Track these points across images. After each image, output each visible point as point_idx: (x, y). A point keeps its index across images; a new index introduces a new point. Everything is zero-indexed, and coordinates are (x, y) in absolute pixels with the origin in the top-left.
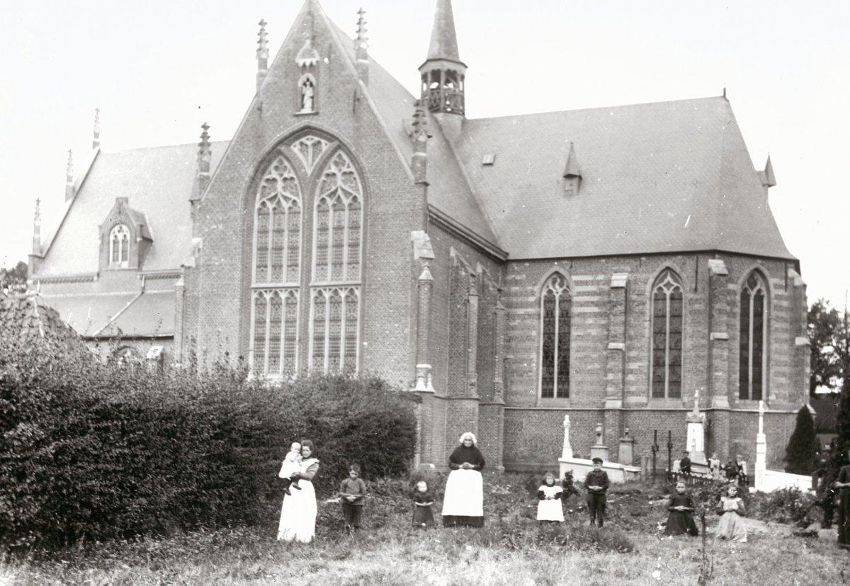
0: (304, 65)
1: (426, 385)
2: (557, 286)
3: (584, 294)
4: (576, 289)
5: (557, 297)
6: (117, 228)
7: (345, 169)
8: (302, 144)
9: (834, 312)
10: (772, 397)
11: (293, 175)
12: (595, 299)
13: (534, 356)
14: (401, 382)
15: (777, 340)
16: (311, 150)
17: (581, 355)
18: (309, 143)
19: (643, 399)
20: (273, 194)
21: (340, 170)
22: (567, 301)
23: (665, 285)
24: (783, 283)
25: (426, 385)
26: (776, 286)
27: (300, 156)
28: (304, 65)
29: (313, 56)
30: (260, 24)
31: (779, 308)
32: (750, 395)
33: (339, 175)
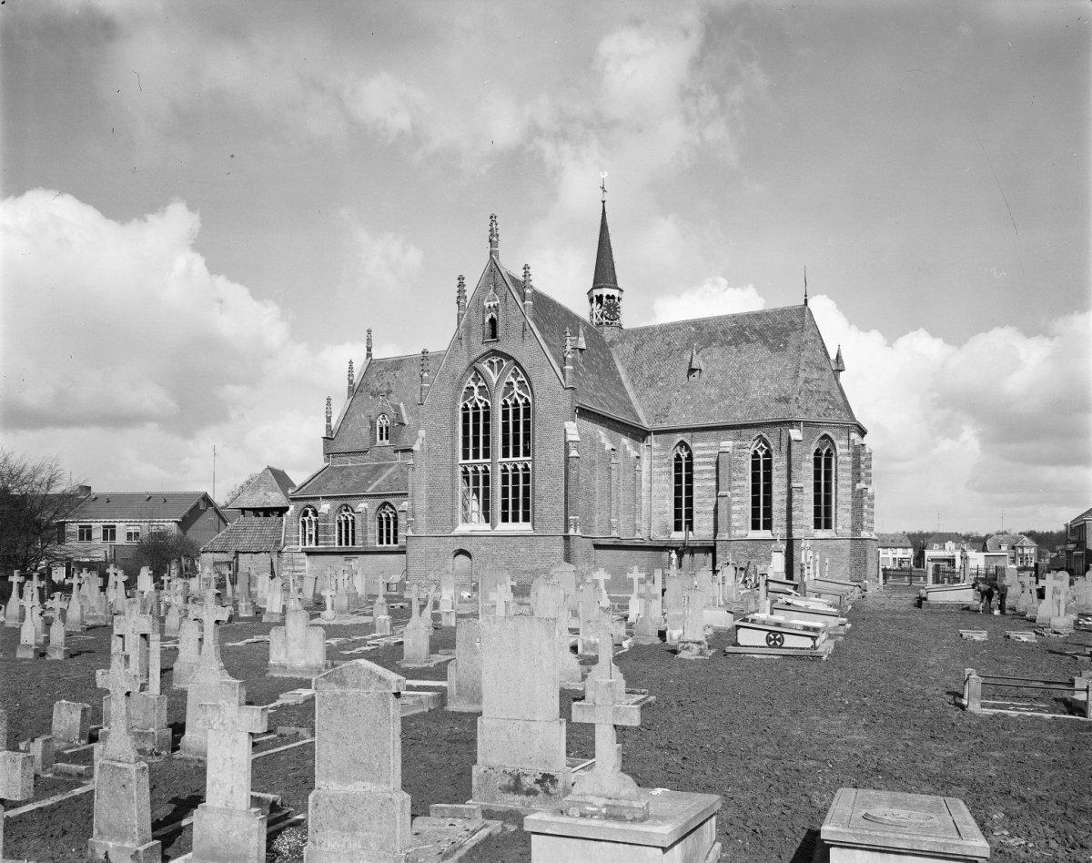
0: (490, 307)
1: (575, 531)
2: (683, 451)
3: (702, 456)
4: (696, 453)
5: (683, 458)
6: (381, 416)
7: (519, 379)
8: (490, 361)
9: (666, 218)
10: (840, 528)
11: (484, 384)
12: (707, 460)
13: (667, 502)
14: (368, 693)
15: (843, 486)
16: (496, 365)
17: (701, 500)
18: (494, 361)
19: (743, 532)
20: (471, 398)
21: (476, 384)
22: (690, 457)
25: (575, 531)
28: (490, 307)
29: (495, 300)
30: (459, 279)
31: (845, 463)
32: (871, 510)
33: (476, 388)
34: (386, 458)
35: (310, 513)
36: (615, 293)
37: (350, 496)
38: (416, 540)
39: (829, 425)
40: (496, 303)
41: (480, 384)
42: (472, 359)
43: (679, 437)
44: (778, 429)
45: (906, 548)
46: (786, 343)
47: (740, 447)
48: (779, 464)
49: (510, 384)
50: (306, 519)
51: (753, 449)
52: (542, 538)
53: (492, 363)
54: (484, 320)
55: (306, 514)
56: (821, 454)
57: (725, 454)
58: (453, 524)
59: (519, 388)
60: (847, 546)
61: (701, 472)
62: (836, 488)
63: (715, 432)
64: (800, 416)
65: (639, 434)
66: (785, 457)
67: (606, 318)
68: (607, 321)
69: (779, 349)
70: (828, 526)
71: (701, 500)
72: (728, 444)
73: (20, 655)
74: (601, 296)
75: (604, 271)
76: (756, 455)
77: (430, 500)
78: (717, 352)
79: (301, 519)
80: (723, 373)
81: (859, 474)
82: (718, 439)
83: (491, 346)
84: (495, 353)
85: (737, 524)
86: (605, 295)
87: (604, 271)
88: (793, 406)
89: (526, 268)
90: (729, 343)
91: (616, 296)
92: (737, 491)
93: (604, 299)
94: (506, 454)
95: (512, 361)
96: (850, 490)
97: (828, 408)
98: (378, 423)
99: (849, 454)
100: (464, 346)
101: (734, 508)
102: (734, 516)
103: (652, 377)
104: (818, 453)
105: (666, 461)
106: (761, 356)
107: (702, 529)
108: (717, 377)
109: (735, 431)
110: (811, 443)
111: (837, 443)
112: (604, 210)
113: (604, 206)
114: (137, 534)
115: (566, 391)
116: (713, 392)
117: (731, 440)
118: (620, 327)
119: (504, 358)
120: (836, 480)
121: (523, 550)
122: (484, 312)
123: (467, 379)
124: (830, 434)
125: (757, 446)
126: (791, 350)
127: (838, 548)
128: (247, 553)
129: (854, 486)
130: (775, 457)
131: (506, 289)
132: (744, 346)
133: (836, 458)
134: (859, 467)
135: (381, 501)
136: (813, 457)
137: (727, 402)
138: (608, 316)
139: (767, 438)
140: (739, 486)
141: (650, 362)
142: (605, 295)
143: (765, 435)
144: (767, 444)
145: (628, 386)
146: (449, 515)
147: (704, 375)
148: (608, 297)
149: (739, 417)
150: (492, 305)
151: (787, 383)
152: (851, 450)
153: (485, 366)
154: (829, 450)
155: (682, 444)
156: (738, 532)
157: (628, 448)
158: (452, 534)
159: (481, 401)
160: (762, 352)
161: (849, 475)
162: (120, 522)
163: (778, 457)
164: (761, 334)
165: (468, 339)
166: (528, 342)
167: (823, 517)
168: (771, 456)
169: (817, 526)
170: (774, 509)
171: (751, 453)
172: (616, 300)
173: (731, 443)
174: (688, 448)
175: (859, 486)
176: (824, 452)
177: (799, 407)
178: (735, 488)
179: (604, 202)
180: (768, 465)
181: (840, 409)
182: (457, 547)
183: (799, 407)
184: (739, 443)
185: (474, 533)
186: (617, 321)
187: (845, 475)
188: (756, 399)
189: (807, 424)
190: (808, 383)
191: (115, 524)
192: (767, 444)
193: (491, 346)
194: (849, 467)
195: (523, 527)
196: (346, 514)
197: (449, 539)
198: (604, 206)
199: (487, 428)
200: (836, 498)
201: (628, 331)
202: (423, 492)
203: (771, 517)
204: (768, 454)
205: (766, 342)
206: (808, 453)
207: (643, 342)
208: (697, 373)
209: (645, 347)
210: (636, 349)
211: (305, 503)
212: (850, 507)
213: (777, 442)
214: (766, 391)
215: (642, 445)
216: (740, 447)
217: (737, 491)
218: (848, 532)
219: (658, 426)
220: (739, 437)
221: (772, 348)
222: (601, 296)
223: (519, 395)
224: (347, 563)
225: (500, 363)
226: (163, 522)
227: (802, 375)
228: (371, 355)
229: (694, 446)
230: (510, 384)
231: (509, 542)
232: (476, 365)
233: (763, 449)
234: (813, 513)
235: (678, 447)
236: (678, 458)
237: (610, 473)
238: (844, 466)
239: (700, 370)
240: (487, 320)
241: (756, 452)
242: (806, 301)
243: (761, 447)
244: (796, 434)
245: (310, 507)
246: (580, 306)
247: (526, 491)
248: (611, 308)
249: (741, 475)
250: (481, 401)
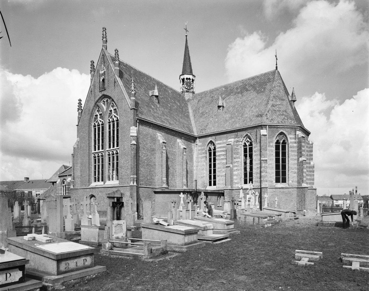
0: (102, 74)
1: (133, 183)
3: (220, 147)
4: (217, 146)
5: (212, 149)
10: (290, 182)
12: (222, 149)
15: (292, 159)
16: (106, 103)
17: (219, 170)
18: (105, 100)
20: (97, 120)
22: (215, 149)
23: (246, 142)
24: (294, 137)
25: (133, 183)
26: (290, 138)
27: (103, 105)
32: (313, 174)
36: (191, 77)
38: (75, 191)
39: (284, 127)
42: (96, 101)
43: (210, 139)
44: (255, 130)
45: (361, 200)
46: (264, 89)
47: (237, 141)
48: (256, 148)
49: (111, 111)
50: (64, 185)
51: (243, 142)
52: (122, 188)
54: (100, 80)
56: (280, 143)
57: (229, 145)
58: (89, 182)
59: (115, 113)
60: (295, 192)
61: (219, 156)
62: (288, 161)
63: (225, 135)
64: (268, 122)
65: (190, 139)
66: (259, 144)
67: (186, 89)
68: (187, 90)
70: (284, 181)
71: (219, 170)
72: (231, 140)
74: (184, 78)
75: (187, 67)
77: (81, 171)
78: (232, 97)
79: (62, 185)
80: (234, 106)
81: (301, 153)
82: (227, 138)
84: (105, 96)
85: (236, 181)
86: (185, 78)
87: (187, 67)
88: (264, 118)
89: (117, 51)
90: (239, 93)
91: (191, 78)
92: (236, 164)
93: (185, 80)
96: (296, 162)
97: (284, 119)
99: (295, 142)
100: (93, 95)
101: (235, 173)
102: (235, 177)
103: (202, 113)
104: (278, 142)
105: (204, 151)
106: (252, 96)
107: (220, 185)
108: (231, 109)
109: (233, 134)
110: (273, 137)
111: (288, 137)
112: (187, 48)
113: (186, 38)
114: (39, 194)
115: (132, 110)
116: (228, 116)
117: (233, 138)
118: (193, 92)
119: (109, 98)
120: (288, 156)
123: (95, 111)
124: (283, 131)
125: (246, 140)
126: (267, 92)
127: (290, 193)
129: (298, 159)
130: (254, 145)
132: (245, 93)
133: (288, 144)
134: (301, 149)
136: (275, 144)
137: (233, 120)
138: (187, 87)
140: (237, 161)
141: (203, 106)
142: (185, 78)
143: (249, 134)
144: (250, 139)
145: (192, 118)
146: (87, 178)
147: (225, 109)
148: (187, 79)
151: (262, 108)
152: (297, 140)
153: (102, 104)
154: (284, 141)
155: (211, 142)
156: (237, 185)
157: (180, 144)
159: (100, 121)
161: (296, 154)
162: (34, 190)
163: (255, 145)
164: (254, 87)
167: (281, 175)
168: (252, 145)
169: (277, 181)
170: (253, 172)
171: (243, 144)
172: (191, 80)
173: (233, 140)
174: (214, 145)
175: (301, 159)
176: (281, 142)
177: (267, 118)
178: (235, 163)
179: (186, 36)
180: (251, 150)
181: (291, 119)
183: (267, 118)
184: (237, 139)
186: (192, 90)
187: (293, 153)
188: (246, 117)
189: (270, 127)
190: (274, 106)
191: (24, 191)
192: (250, 139)
194: (296, 149)
197: (88, 190)
198: (186, 38)
200: (288, 166)
201: (199, 94)
202: (78, 168)
203: (252, 177)
204: (251, 144)
206: (272, 142)
207: (202, 98)
208: (221, 108)
209: (203, 100)
210: (199, 102)
212: (296, 171)
213: (255, 137)
214: (252, 112)
215: (193, 144)
216: (237, 141)
217: (236, 164)
218: (295, 184)
219: (202, 134)
220: (237, 136)
221: (258, 92)
222: (184, 78)
225: (107, 101)
226: (40, 190)
227: (271, 103)
229: (216, 143)
230: (111, 111)
231: (110, 190)
233: (249, 141)
234: (275, 174)
235: (210, 144)
236: (210, 150)
237: (162, 154)
238: (293, 149)
239: (223, 107)
240: (101, 80)
241: (245, 143)
242: (277, 67)
243: (248, 140)
244: (264, 132)
246: (178, 87)
247: (117, 163)
248: (188, 84)
249: (238, 156)
250: (100, 121)
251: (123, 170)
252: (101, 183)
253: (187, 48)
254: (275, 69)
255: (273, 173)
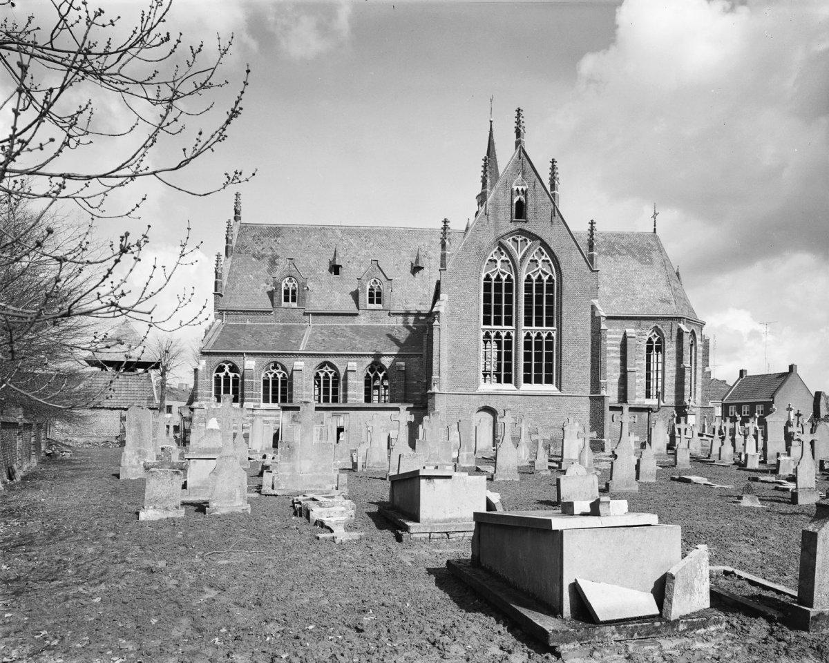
0: (517, 190)
6: (287, 279)
7: (543, 258)
8: (514, 239)
18: (519, 239)
28: (517, 190)
29: (525, 185)
34: (293, 319)
35: (227, 369)
37: (283, 354)
40: (524, 189)
41: (503, 258)
44: (669, 322)
47: (640, 334)
50: (222, 375)
52: (569, 398)
53: (517, 241)
55: (221, 369)
57: (632, 339)
69: (646, 263)
73: (147, 515)
76: (650, 341)
77: (453, 360)
83: (519, 225)
94: (528, 322)
95: (539, 242)
98: (283, 285)
100: (492, 222)
112: (491, 129)
121: (550, 408)
122: (512, 194)
125: (651, 334)
128: (114, 409)
131: (535, 177)
135: (320, 360)
139: (661, 329)
143: (659, 327)
149: (636, 311)
150: (520, 189)
158: (477, 392)
160: (634, 264)
165: (495, 216)
166: (556, 228)
179: (491, 122)
182: (482, 404)
184: (639, 331)
185: (500, 392)
193: (519, 225)
195: (551, 388)
196: (275, 371)
199: (509, 299)
205: (634, 256)
211: (222, 358)
216: (640, 334)
223: (542, 272)
224: (335, 418)
228: (240, 219)
231: (535, 401)
232: (502, 240)
242: (655, 229)
243: (655, 335)
245: (227, 362)
251: (570, 368)
252: (509, 387)
253: (491, 129)
254: (653, 231)
255: (615, 378)
